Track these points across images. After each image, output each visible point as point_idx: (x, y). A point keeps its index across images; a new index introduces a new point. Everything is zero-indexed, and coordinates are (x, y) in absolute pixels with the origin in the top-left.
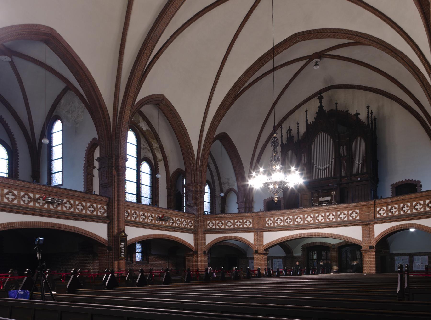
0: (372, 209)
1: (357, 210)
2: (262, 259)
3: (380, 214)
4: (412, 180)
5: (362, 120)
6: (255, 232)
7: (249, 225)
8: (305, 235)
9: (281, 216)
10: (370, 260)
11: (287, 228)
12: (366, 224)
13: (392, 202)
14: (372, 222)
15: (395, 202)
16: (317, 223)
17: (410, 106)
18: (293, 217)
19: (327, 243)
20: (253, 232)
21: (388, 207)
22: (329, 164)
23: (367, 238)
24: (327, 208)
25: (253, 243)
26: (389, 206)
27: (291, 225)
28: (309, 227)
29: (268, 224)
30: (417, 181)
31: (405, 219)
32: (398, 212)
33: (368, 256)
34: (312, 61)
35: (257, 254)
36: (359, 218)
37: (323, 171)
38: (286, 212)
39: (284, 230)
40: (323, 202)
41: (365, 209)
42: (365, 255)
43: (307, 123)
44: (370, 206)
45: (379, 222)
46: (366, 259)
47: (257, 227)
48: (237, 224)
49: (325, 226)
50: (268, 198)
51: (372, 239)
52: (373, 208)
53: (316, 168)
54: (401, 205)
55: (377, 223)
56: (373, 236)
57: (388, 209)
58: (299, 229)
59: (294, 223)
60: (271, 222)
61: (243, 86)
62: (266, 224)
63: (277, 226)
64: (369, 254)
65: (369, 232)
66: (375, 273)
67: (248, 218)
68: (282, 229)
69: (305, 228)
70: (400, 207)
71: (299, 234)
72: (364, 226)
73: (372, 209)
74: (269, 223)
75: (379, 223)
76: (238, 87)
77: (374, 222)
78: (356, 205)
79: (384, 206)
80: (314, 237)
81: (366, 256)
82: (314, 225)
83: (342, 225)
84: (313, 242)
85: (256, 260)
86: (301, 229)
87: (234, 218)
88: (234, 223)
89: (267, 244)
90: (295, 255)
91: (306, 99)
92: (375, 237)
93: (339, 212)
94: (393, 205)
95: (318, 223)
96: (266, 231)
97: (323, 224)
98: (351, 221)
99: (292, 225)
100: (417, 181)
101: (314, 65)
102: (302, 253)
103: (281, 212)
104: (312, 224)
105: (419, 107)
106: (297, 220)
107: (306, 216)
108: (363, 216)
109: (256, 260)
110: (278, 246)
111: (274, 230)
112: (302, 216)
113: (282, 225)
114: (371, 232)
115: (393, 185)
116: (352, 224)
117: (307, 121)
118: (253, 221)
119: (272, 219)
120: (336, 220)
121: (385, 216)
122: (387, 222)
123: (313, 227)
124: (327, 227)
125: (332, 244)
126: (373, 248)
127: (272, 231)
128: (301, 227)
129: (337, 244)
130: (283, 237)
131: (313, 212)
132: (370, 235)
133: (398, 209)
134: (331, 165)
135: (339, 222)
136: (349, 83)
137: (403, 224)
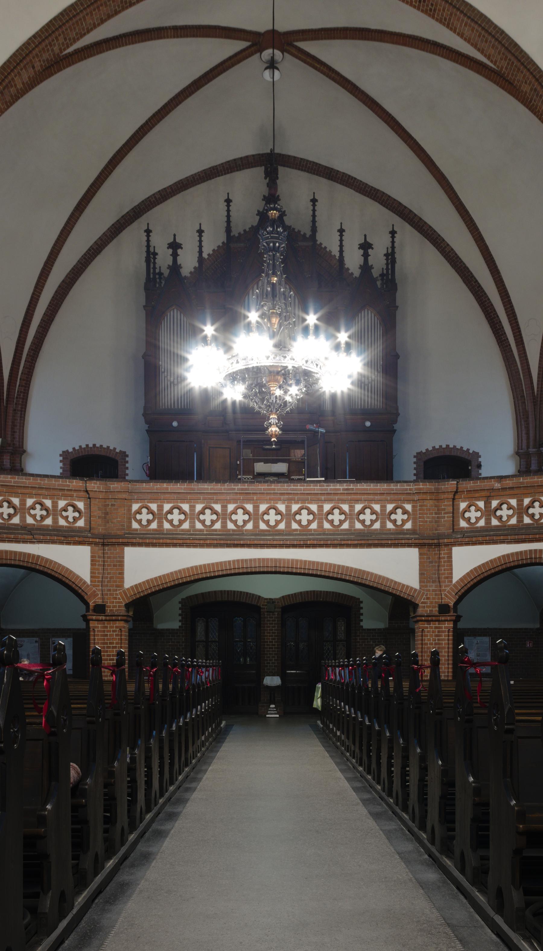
0: (447, 505)
1: (407, 503)
2: (117, 635)
3: (468, 520)
4: (462, 448)
5: (350, 272)
6: (96, 544)
7: (75, 519)
8: (259, 563)
9: (183, 501)
10: (439, 644)
11: (206, 539)
12: (430, 545)
13: (504, 489)
14: (449, 540)
15: (511, 492)
16: (296, 530)
17: (464, 264)
18: (224, 507)
20: (89, 544)
21: (490, 503)
23: (433, 582)
24: (326, 490)
25: (89, 582)
26: (494, 499)
27: (216, 530)
28: (275, 542)
29: (139, 522)
30: (471, 451)
31: (537, 536)
32: (518, 518)
33: (433, 632)
34: (261, 51)
35: (100, 618)
36: (412, 526)
38: (204, 489)
39: (195, 546)
40: (263, 476)
41: (429, 503)
42: (427, 628)
44: (442, 496)
45: (467, 540)
46: (429, 640)
47: (101, 530)
48: (32, 512)
49: (322, 542)
50: (77, 448)
51: (446, 586)
52: (451, 503)
54: (527, 501)
55: (461, 544)
56: (447, 578)
57: (491, 507)
58: (242, 546)
59: (224, 525)
61: (75, 40)
62: (165, 522)
63: (170, 530)
64: (436, 628)
65: (439, 566)
66: (450, 678)
67: (72, 496)
68: (188, 541)
69: (262, 542)
70: (523, 504)
71: (242, 560)
72: (425, 550)
73: (449, 505)
74: (141, 520)
75: (467, 544)
76: (61, 39)
77: (452, 540)
78: (406, 489)
79: (478, 499)
80: (219, 576)
81: (428, 632)
82: (286, 535)
83: (370, 542)
85: (98, 635)
86: (249, 546)
87: (23, 491)
88: (25, 509)
89: (136, 585)
90: (161, 626)
91: (201, 172)
92: (455, 580)
93: (358, 503)
94: (503, 499)
95: (300, 530)
96: (133, 545)
98: (392, 534)
99: (220, 530)
100: (471, 451)
101: (266, 69)
102: (180, 621)
103: (185, 489)
104: (280, 533)
105: (489, 268)
106: (234, 517)
107: (263, 507)
108: (422, 522)
109: (98, 635)
111: (161, 541)
112: (250, 507)
113: (188, 531)
114: (444, 566)
115: (419, 455)
116: (396, 542)
118: (88, 506)
119: (154, 507)
120: (350, 526)
121: (481, 527)
122: (488, 543)
123: (288, 543)
124: (327, 546)
125: (267, 599)
126: (449, 612)
127: (154, 545)
128: (250, 540)
129: (280, 599)
130: (192, 568)
131: (286, 497)
132: (439, 574)
133: (518, 509)
135: (359, 533)
136: (324, 162)
137: (531, 551)
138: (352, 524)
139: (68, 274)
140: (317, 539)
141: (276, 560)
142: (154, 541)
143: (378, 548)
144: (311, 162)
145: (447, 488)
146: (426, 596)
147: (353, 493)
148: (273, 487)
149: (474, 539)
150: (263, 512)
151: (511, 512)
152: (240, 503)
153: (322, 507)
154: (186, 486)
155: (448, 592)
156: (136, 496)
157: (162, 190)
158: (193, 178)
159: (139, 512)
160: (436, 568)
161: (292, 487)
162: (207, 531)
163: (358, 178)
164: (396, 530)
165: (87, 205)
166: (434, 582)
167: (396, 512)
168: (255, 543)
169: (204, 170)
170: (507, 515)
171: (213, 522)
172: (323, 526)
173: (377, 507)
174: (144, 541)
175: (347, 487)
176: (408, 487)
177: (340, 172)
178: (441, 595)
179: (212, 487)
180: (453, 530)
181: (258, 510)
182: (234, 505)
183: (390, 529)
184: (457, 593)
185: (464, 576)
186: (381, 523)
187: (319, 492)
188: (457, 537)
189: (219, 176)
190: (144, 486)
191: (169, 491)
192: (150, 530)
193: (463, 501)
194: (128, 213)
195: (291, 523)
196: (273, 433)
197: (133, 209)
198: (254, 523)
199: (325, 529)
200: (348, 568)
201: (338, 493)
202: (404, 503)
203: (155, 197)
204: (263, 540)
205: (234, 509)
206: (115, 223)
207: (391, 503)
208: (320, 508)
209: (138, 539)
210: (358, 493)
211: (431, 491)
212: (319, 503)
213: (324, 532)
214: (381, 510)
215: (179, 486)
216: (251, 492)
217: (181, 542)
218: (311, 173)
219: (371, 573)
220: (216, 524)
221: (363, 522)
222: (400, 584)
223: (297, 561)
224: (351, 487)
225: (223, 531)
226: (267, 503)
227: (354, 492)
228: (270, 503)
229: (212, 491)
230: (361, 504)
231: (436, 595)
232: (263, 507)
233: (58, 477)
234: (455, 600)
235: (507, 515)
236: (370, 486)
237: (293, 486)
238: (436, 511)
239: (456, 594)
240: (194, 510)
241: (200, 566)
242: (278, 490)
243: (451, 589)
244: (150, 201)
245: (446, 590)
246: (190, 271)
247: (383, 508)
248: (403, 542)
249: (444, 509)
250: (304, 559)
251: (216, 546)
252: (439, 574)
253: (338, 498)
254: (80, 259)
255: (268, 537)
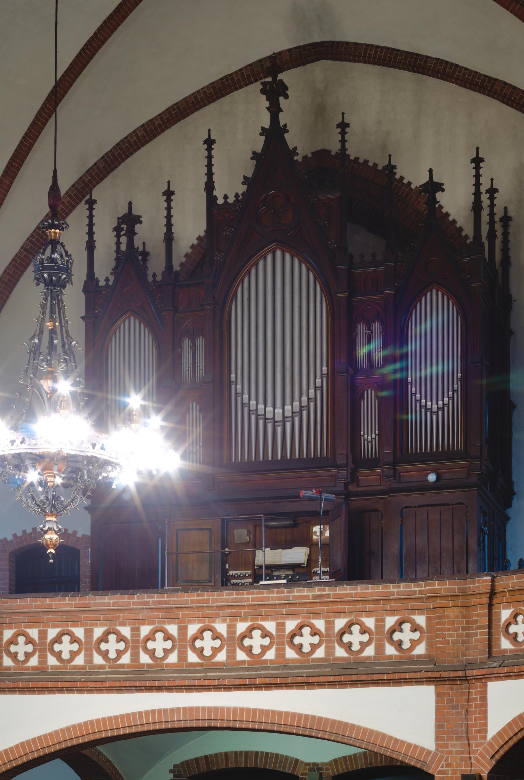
5: (451, 218)
12: (453, 680)
14: (480, 672)
16: (243, 662)
18: (135, 631)
19: (287, 757)
22: (304, 399)
24: (287, 598)
27: (123, 666)
28: (206, 683)
36: (427, 649)
37: (279, 430)
38: (103, 604)
41: (452, 613)
43: (211, 199)
44: (473, 601)
45: (506, 670)
49: (278, 681)
51: (477, 745)
52: (486, 611)
53: (246, 409)
55: (499, 678)
56: (479, 731)
58: (159, 689)
59: (135, 657)
60: (30, 648)
62: (49, 656)
63: (56, 667)
65: (467, 713)
68: (78, 684)
69: (187, 683)
72: (446, 688)
73: (482, 615)
75: (508, 677)
77: (485, 671)
78: (414, 592)
83: (354, 678)
84: (226, 754)
86: (169, 689)
91: (208, 86)
93: (340, 617)
97: (267, 669)
99: (128, 666)
103: (76, 605)
104: (220, 667)
108: (441, 643)
110: (58, 762)
111: (40, 685)
112: (173, 629)
113: (83, 667)
114: (475, 712)
116: (396, 676)
117: (210, 186)
120: (326, 653)
123: (226, 682)
129: (330, 763)
130: (86, 723)
132: (467, 726)
134: (312, 404)
135: (341, 664)
138: (330, 650)
139: (8, 268)
140: (271, 676)
141: (210, 709)
142: (31, 685)
143: (369, 687)
144: (382, 48)
145: (478, 587)
146: (445, 761)
147: (330, 602)
148: (205, 597)
149: (516, 669)
150: (193, 635)
151: (416, 636)
152: (158, 624)
153: (283, 624)
154: (77, 602)
155: (481, 754)
156: (8, 619)
157: (147, 123)
158: (195, 97)
159: (13, 641)
160: (464, 716)
161: (235, 596)
162: (110, 667)
163: (461, 64)
164: (401, 657)
165: (21, 165)
166: (459, 738)
167: (401, 629)
168: (177, 684)
169: (211, 84)
170: (411, 640)
171: (120, 653)
172: (284, 655)
173: (370, 622)
174: (15, 685)
175: (319, 593)
176: (418, 589)
177: (432, 58)
178: (471, 760)
179: (116, 601)
180: (490, 653)
181: (186, 634)
182: (150, 627)
183: (390, 657)
184: (493, 756)
185: (504, 729)
186: (376, 647)
187: (276, 602)
188: (492, 666)
189: (237, 89)
190: (18, 603)
191: (54, 609)
192: (28, 668)
193: (505, 608)
194: (95, 164)
195: (235, 652)
196: (49, 542)
197: (103, 157)
198: (179, 653)
199: (289, 659)
200: (320, 719)
201: (306, 603)
202: (414, 614)
203: (137, 136)
204: (189, 679)
205: (150, 633)
206: (77, 182)
207: (394, 615)
208: (281, 627)
209: (7, 682)
210: (337, 601)
211: (453, 594)
212: (278, 619)
213: (286, 664)
214: (377, 627)
215: (67, 602)
216: (174, 606)
217: (69, 685)
218: (383, 65)
219: (358, 726)
220: (123, 657)
221: (348, 646)
222: (403, 742)
223: (242, 710)
224: (327, 592)
225: (134, 667)
226: (200, 622)
227: (331, 600)
228: (204, 622)
229: (115, 608)
230: (344, 617)
231: (462, 759)
232: (193, 629)
233: (179, 554)
234: (490, 768)
235: (411, 640)
236: (357, 589)
237: (237, 594)
238: (464, 625)
239: (492, 758)
240: (91, 637)
241: (98, 720)
242: (214, 601)
243: (485, 749)
244: (129, 142)
245: (477, 751)
246: (191, 245)
247: (380, 622)
248: (407, 676)
249: (476, 621)
250: (252, 706)
251: (120, 690)
252: (467, 726)
253: (307, 611)
254: (25, 243)
255: (198, 675)
